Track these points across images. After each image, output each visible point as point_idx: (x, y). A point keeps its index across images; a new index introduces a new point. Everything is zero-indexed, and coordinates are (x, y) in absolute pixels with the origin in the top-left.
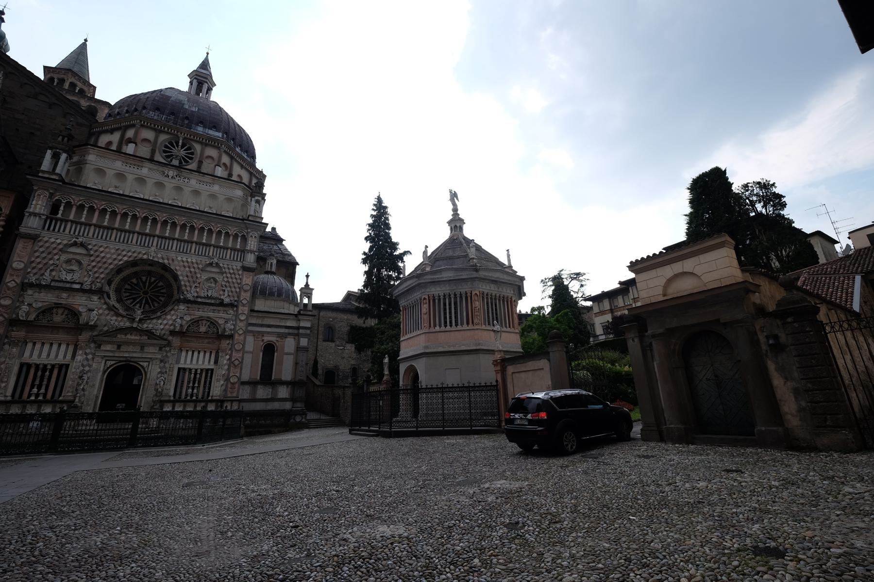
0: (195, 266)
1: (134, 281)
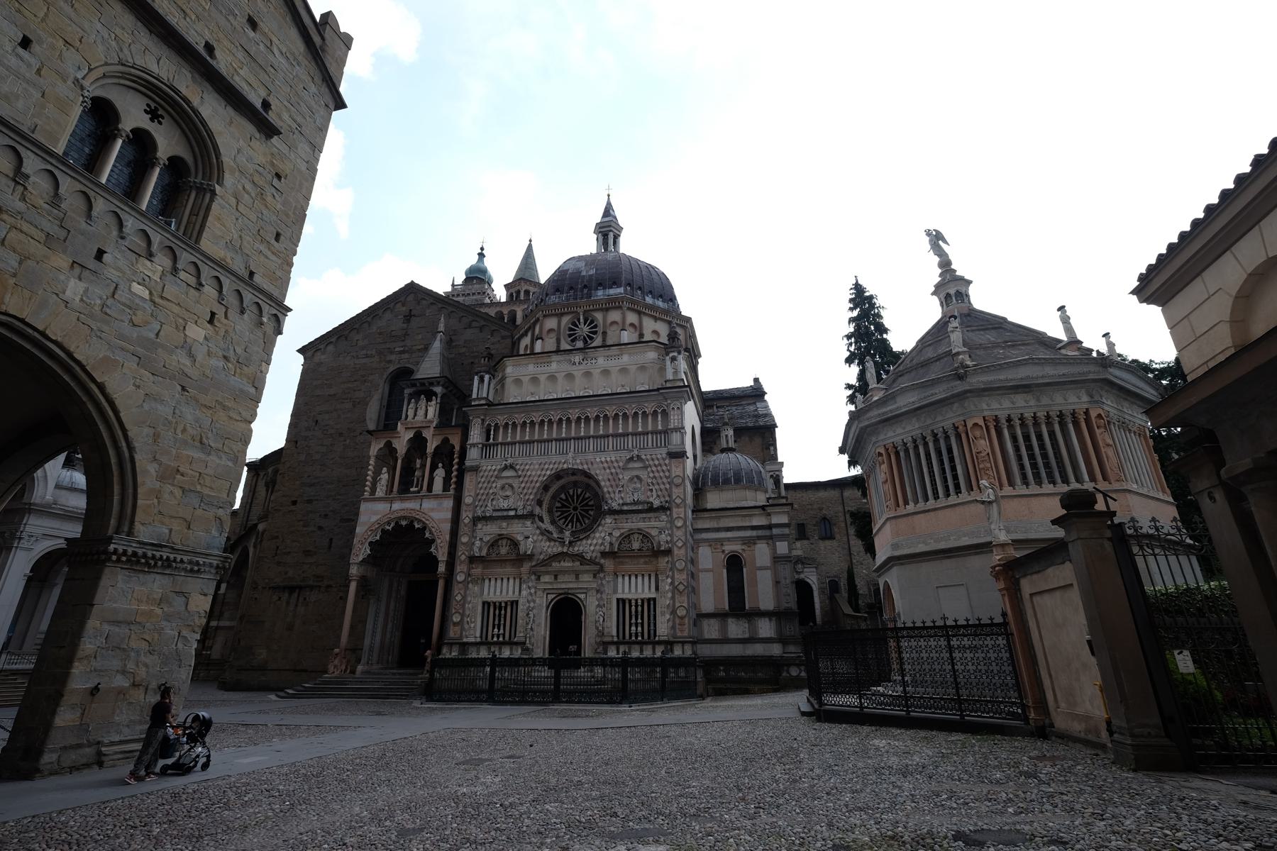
0: (616, 464)
1: (563, 496)
